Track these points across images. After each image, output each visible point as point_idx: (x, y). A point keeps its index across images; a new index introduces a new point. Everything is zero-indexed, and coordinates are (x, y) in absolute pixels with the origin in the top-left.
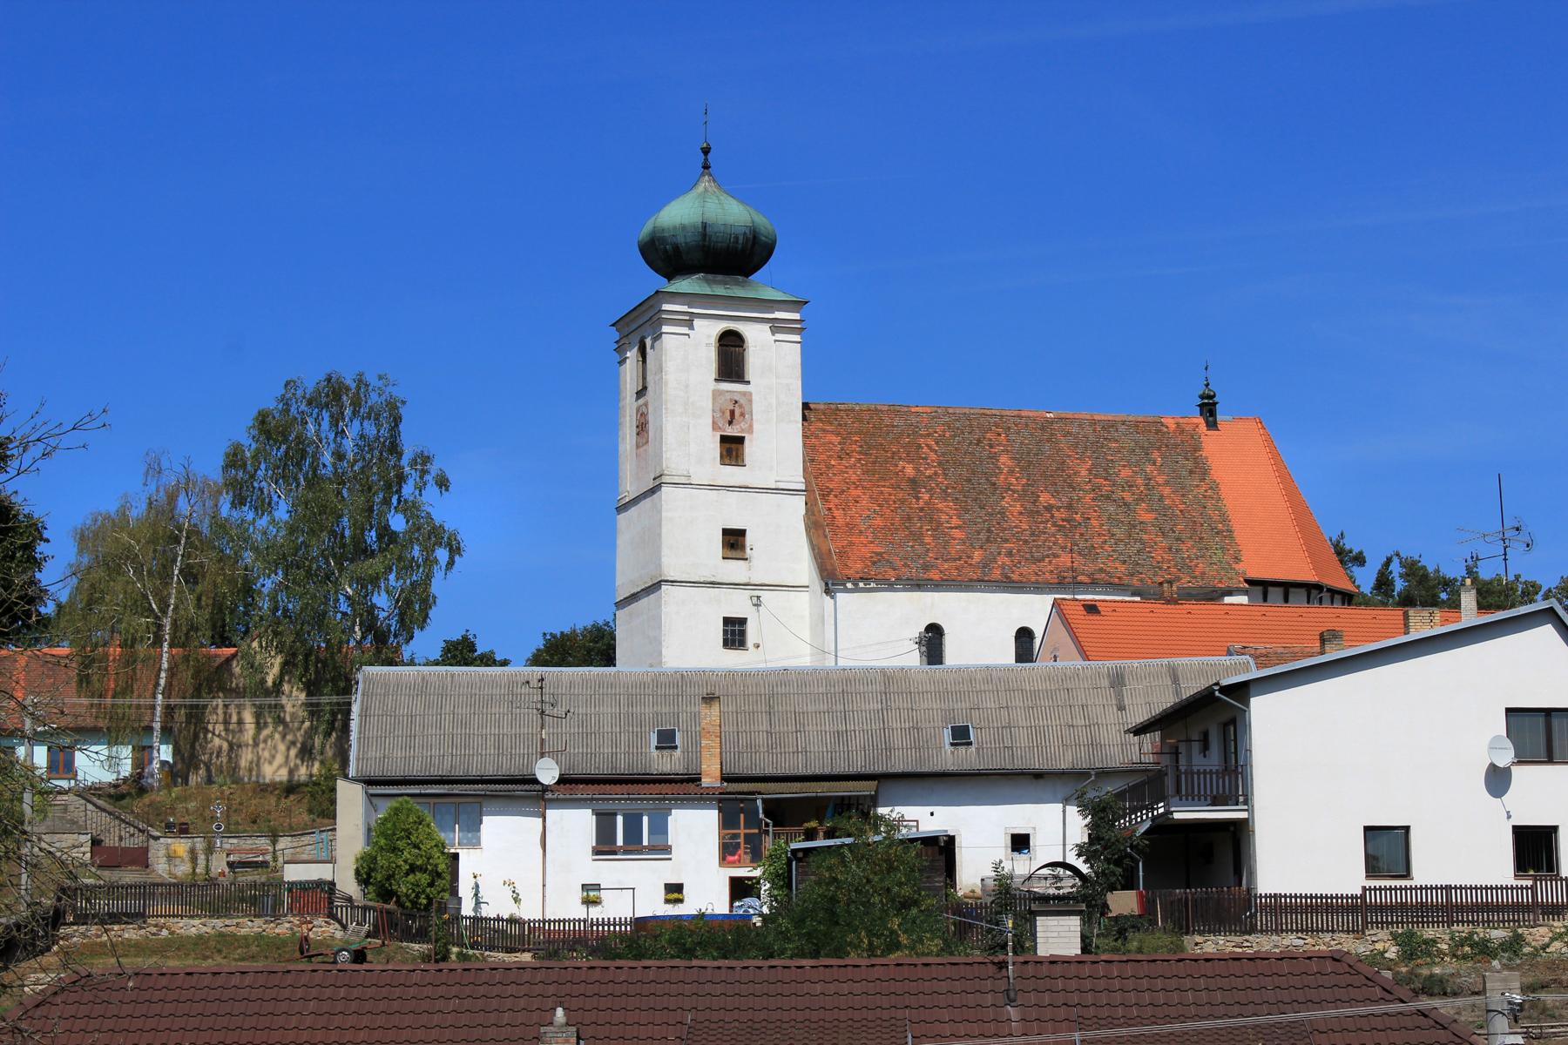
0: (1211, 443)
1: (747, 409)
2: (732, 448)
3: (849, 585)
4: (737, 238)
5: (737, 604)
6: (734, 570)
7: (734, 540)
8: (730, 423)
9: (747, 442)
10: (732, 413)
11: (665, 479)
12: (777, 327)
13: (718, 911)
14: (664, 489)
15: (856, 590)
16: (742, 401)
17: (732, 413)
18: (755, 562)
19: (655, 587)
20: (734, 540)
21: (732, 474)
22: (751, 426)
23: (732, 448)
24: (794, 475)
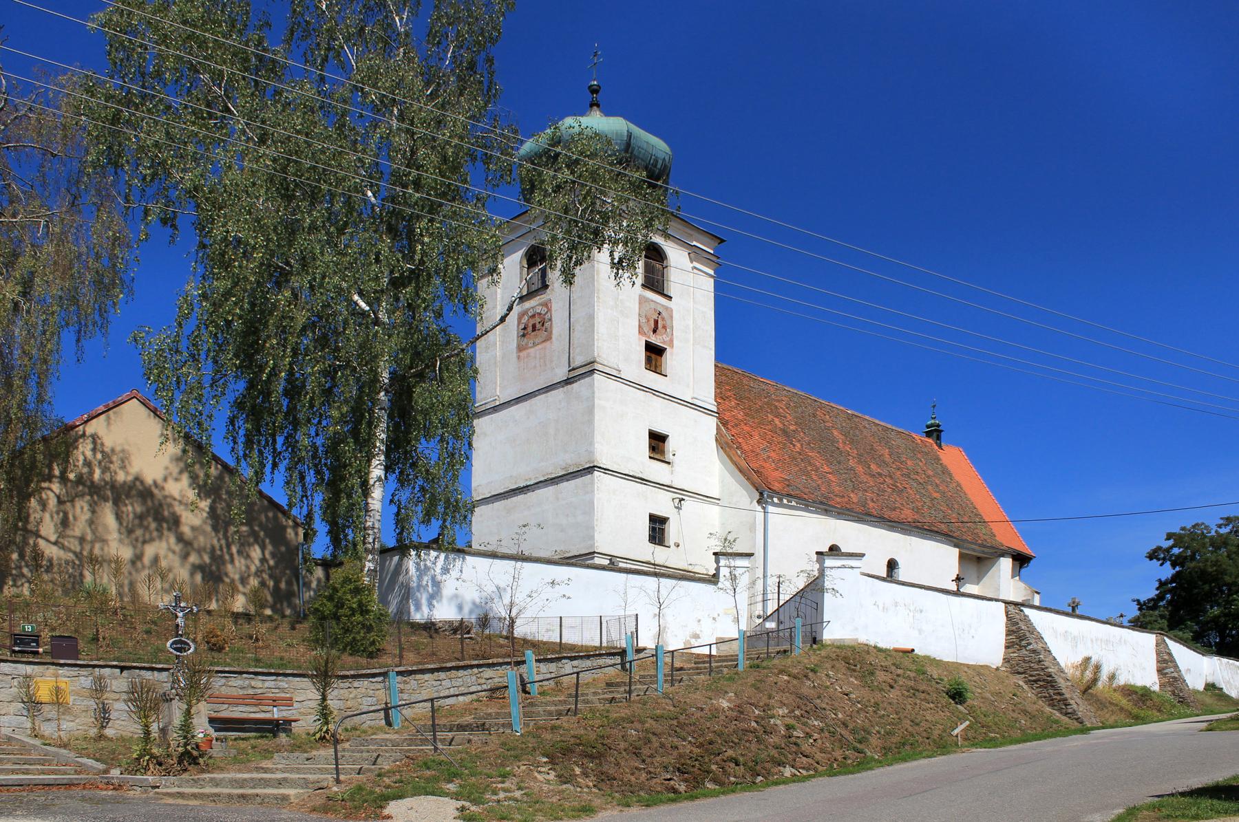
0: (941, 454)
1: (668, 323)
2: (654, 353)
3: (776, 500)
4: (656, 161)
5: (662, 504)
6: (656, 470)
7: (657, 441)
8: (654, 331)
9: (668, 354)
10: (656, 322)
11: (597, 366)
12: (695, 254)
13: (825, 632)
14: (596, 376)
15: (781, 505)
16: (664, 314)
17: (656, 322)
18: (676, 467)
19: (590, 470)
20: (657, 441)
21: (651, 379)
22: (671, 341)
23: (654, 353)
24: (707, 395)
